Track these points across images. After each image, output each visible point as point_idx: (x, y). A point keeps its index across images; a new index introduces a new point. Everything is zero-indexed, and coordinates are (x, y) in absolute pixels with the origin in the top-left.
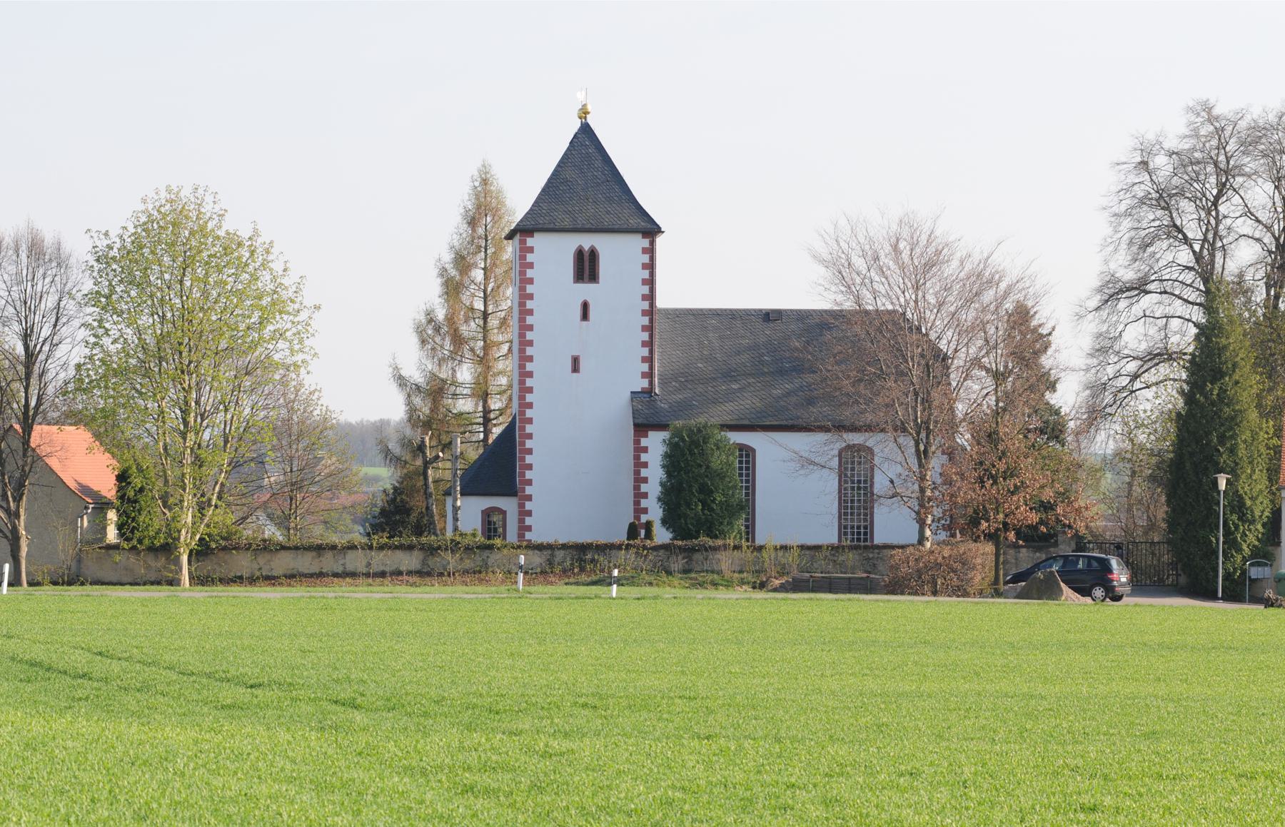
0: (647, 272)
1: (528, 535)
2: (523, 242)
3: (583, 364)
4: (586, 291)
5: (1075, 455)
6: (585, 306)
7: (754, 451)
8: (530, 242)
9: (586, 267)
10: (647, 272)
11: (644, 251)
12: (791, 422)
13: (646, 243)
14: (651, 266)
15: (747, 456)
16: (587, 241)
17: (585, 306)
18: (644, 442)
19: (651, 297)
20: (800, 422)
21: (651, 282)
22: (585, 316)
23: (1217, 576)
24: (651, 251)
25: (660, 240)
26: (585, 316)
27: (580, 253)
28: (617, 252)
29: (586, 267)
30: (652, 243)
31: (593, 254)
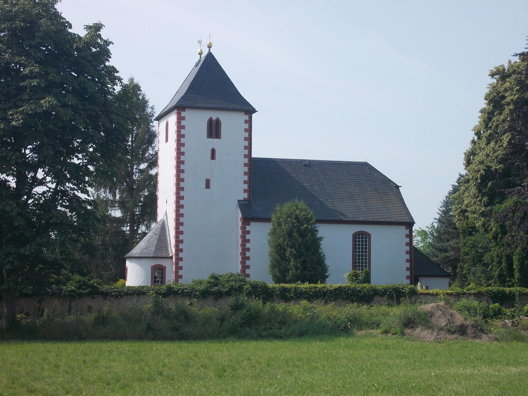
0: (182, 142)
1: (180, 281)
2: (179, 114)
3: (212, 185)
4: (214, 142)
5: (482, 239)
6: (213, 151)
7: (369, 235)
8: (183, 114)
9: (214, 130)
10: (182, 142)
11: (246, 122)
12: (329, 218)
13: (247, 117)
14: (249, 130)
15: (366, 238)
16: (214, 115)
17: (213, 151)
18: (248, 228)
19: (249, 148)
20: (343, 218)
21: (249, 139)
22: (213, 157)
23: (287, 283)
24: (249, 122)
25: (254, 115)
26: (213, 157)
27: (210, 121)
28: (231, 122)
29: (214, 130)
30: (251, 118)
31: (218, 122)
